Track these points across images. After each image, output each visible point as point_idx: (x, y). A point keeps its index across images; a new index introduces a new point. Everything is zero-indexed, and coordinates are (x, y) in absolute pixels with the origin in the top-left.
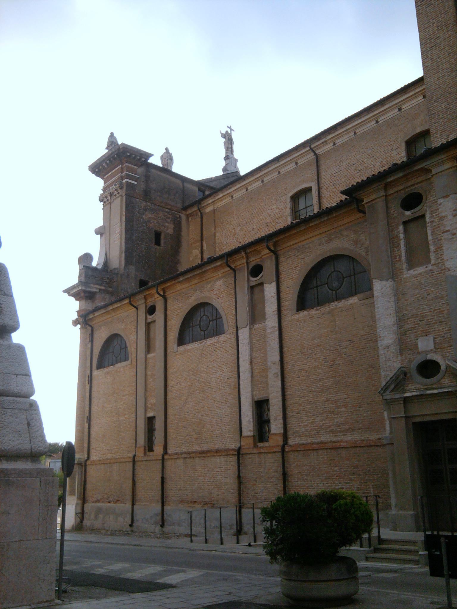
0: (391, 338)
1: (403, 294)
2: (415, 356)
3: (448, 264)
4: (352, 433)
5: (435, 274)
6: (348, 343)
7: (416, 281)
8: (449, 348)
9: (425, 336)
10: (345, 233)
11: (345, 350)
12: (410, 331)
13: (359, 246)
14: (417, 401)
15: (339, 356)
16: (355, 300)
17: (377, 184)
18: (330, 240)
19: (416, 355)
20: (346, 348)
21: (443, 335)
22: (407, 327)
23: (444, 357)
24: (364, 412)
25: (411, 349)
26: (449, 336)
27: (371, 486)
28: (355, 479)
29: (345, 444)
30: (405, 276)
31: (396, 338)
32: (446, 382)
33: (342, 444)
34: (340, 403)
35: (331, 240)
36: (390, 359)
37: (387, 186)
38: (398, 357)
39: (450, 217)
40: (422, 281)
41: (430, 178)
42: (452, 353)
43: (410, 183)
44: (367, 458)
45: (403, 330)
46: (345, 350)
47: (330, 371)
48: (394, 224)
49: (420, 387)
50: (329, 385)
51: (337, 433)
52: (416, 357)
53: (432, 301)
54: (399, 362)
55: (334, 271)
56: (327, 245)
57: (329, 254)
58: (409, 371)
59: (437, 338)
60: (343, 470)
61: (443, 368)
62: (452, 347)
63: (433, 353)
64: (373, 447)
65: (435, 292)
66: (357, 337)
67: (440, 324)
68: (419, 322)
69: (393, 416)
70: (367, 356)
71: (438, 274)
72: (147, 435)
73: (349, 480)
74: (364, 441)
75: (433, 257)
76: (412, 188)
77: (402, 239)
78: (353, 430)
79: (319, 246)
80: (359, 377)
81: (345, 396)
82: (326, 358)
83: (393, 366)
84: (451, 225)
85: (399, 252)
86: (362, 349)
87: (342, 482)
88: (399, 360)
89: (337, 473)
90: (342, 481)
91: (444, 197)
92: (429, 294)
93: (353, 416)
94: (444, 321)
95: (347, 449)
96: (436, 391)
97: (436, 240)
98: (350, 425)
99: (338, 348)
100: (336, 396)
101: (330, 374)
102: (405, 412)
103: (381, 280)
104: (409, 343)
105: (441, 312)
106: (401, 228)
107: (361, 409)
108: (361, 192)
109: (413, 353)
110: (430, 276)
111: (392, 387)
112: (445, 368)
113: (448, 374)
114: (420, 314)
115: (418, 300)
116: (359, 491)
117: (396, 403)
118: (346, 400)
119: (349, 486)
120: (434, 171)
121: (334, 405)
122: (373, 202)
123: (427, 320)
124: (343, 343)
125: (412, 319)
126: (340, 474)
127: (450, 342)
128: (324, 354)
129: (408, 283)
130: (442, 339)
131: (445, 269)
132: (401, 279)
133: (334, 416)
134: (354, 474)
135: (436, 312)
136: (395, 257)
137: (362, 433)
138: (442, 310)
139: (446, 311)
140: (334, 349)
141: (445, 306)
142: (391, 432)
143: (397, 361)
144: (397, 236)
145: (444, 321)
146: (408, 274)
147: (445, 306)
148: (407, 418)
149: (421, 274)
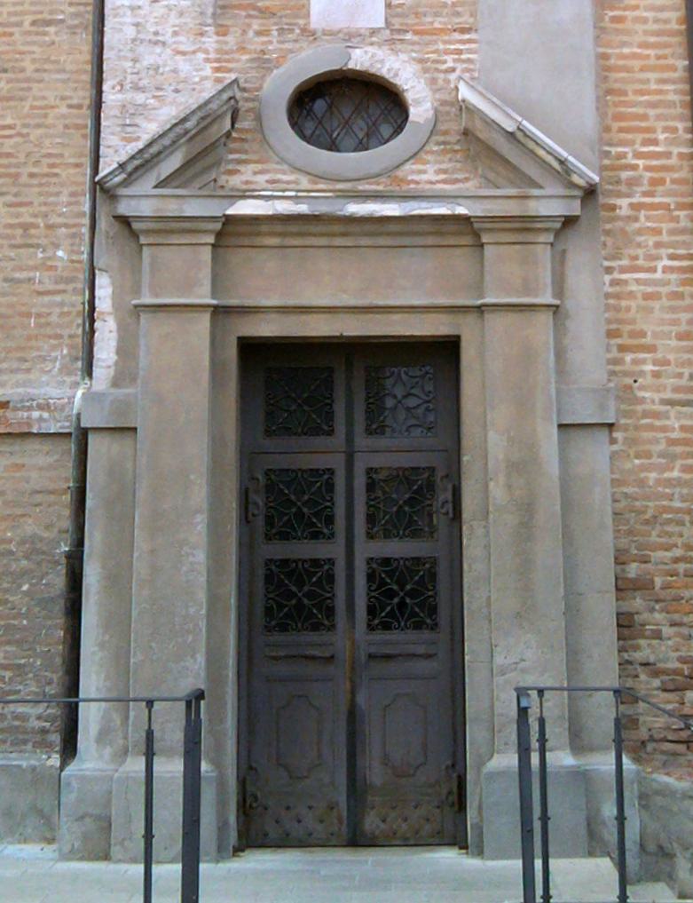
2: (286, 46)
8: (457, 36)
19: (296, 41)
32: (424, 177)
36: (160, 38)
38: (202, 34)
42: (469, 61)
49: (296, 182)
52: (291, 51)
54: (207, 60)
58: (251, 105)
63: (380, 45)
72: (316, 340)
83: (175, 71)
88: (206, 52)
102: (216, 286)
111: (173, 162)
112: (431, 114)
113: (438, 144)
117: (175, 239)
143: (194, 52)
148: (220, 313)
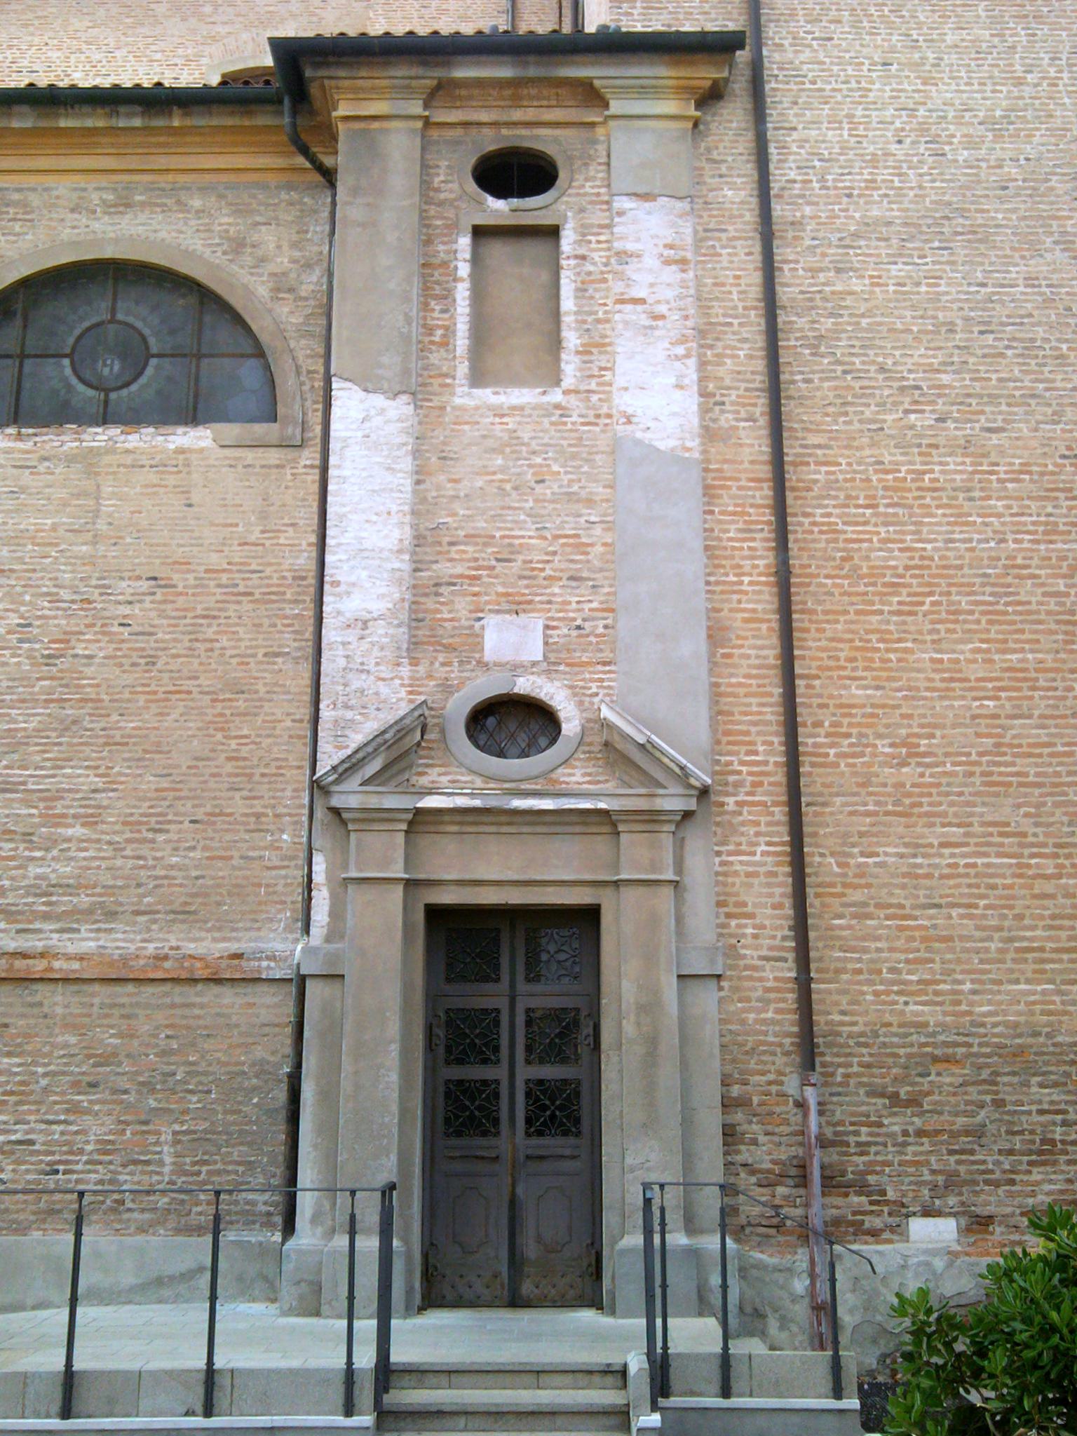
0: (381, 597)
1: (444, 458)
3: (624, 402)
4: (103, 926)
5: (573, 423)
6: (145, 585)
7: (498, 427)
8: (600, 668)
9: (508, 612)
10: (197, 203)
11: (126, 610)
12: (454, 584)
13: (249, 260)
14: (455, 828)
15: (94, 625)
16: (200, 438)
17: (414, 71)
18: (124, 204)
20: (130, 603)
21: (579, 622)
22: (445, 569)
23: (575, 692)
24: (176, 849)
25: (449, 648)
26: (601, 630)
27: (167, 1137)
28: (96, 1108)
29: (76, 965)
30: (458, 401)
31: (403, 600)
32: (573, 779)
33: (57, 964)
34: (68, 807)
35: (128, 205)
37: (440, 92)
38: (398, 665)
39: (650, 261)
40: (519, 434)
41: (592, 125)
42: (609, 687)
43: (517, 115)
44: (167, 1026)
45: (430, 578)
46: (126, 610)
47: (39, 679)
48: (439, 223)
50: (25, 729)
51: (30, 922)
53: (551, 506)
54: (402, 685)
55: (113, 320)
56: (106, 218)
57: (109, 253)
59: (554, 628)
60: (40, 1070)
61: (570, 726)
62: (613, 668)
63: (539, 674)
64: (200, 987)
65: (566, 478)
66: (188, 571)
67: (574, 584)
68: (493, 563)
69: (354, 874)
70: (223, 648)
71: (583, 424)
73: (67, 1111)
74: (166, 958)
75: (570, 367)
76: (524, 132)
77: (462, 280)
78: (112, 915)
79: (73, 211)
80: (173, 717)
81: (99, 782)
82: (29, 625)
83: (377, 694)
84: (652, 285)
85: (446, 316)
86: (204, 617)
87: (32, 1118)
88: (402, 678)
89: (8, 1082)
90: (30, 1112)
91: (635, 195)
92: (542, 481)
93: (119, 862)
94: (589, 579)
95: (75, 988)
96: (547, 804)
97: (590, 319)
98: (100, 895)
99: (96, 597)
100: (53, 776)
101: (36, 689)
102: (408, 863)
103: (366, 390)
104: (446, 624)
105: (582, 548)
106: (465, 242)
107: (161, 838)
108: (342, 73)
109: (461, 663)
110: (552, 424)
114: (503, 537)
115: (499, 488)
116: (106, 1153)
117: (376, 827)
118: (97, 796)
119: (62, 1133)
120: (616, 107)
121: (34, 811)
122: (376, 125)
123: (525, 562)
124: (124, 584)
125: (470, 549)
126: (22, 1083)
127: (601, 650)
128: (23, 609)
129: (466, 427)
130: (575, 633)
131: (609, 416)
132: (443, 408)
133: (27, 853)
134: (93, 1085)
135: (564, 545)
136: (430, 331)
137: (149, 930)
138: (584, 540)
139: (599, 549)
140: (75, 597)
141: (598, 530)
142: (334, 933)
144: (445, 264)
145: (589, 579)
146: (465, 397)
147: (598, 530)
149: (522, 408)
